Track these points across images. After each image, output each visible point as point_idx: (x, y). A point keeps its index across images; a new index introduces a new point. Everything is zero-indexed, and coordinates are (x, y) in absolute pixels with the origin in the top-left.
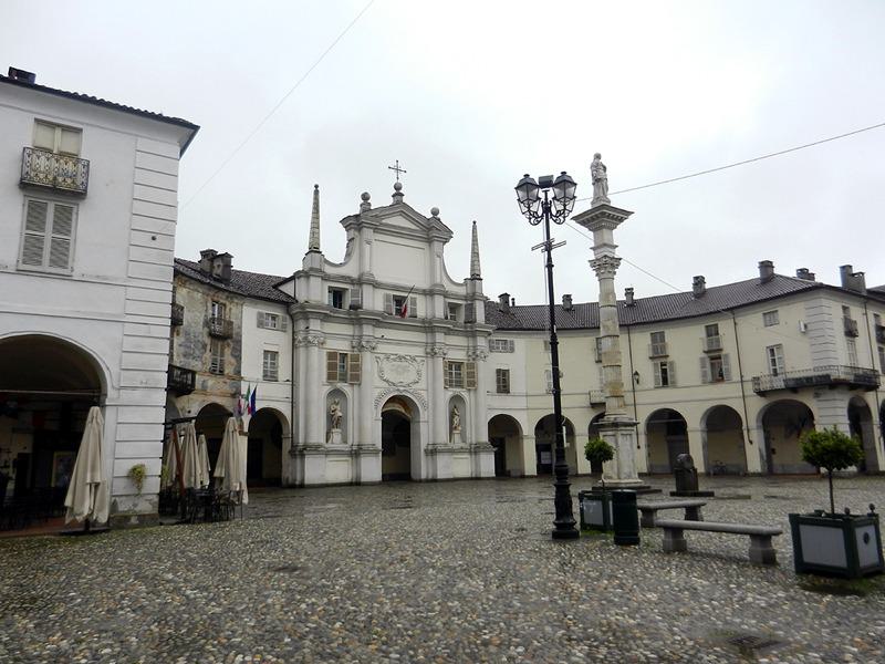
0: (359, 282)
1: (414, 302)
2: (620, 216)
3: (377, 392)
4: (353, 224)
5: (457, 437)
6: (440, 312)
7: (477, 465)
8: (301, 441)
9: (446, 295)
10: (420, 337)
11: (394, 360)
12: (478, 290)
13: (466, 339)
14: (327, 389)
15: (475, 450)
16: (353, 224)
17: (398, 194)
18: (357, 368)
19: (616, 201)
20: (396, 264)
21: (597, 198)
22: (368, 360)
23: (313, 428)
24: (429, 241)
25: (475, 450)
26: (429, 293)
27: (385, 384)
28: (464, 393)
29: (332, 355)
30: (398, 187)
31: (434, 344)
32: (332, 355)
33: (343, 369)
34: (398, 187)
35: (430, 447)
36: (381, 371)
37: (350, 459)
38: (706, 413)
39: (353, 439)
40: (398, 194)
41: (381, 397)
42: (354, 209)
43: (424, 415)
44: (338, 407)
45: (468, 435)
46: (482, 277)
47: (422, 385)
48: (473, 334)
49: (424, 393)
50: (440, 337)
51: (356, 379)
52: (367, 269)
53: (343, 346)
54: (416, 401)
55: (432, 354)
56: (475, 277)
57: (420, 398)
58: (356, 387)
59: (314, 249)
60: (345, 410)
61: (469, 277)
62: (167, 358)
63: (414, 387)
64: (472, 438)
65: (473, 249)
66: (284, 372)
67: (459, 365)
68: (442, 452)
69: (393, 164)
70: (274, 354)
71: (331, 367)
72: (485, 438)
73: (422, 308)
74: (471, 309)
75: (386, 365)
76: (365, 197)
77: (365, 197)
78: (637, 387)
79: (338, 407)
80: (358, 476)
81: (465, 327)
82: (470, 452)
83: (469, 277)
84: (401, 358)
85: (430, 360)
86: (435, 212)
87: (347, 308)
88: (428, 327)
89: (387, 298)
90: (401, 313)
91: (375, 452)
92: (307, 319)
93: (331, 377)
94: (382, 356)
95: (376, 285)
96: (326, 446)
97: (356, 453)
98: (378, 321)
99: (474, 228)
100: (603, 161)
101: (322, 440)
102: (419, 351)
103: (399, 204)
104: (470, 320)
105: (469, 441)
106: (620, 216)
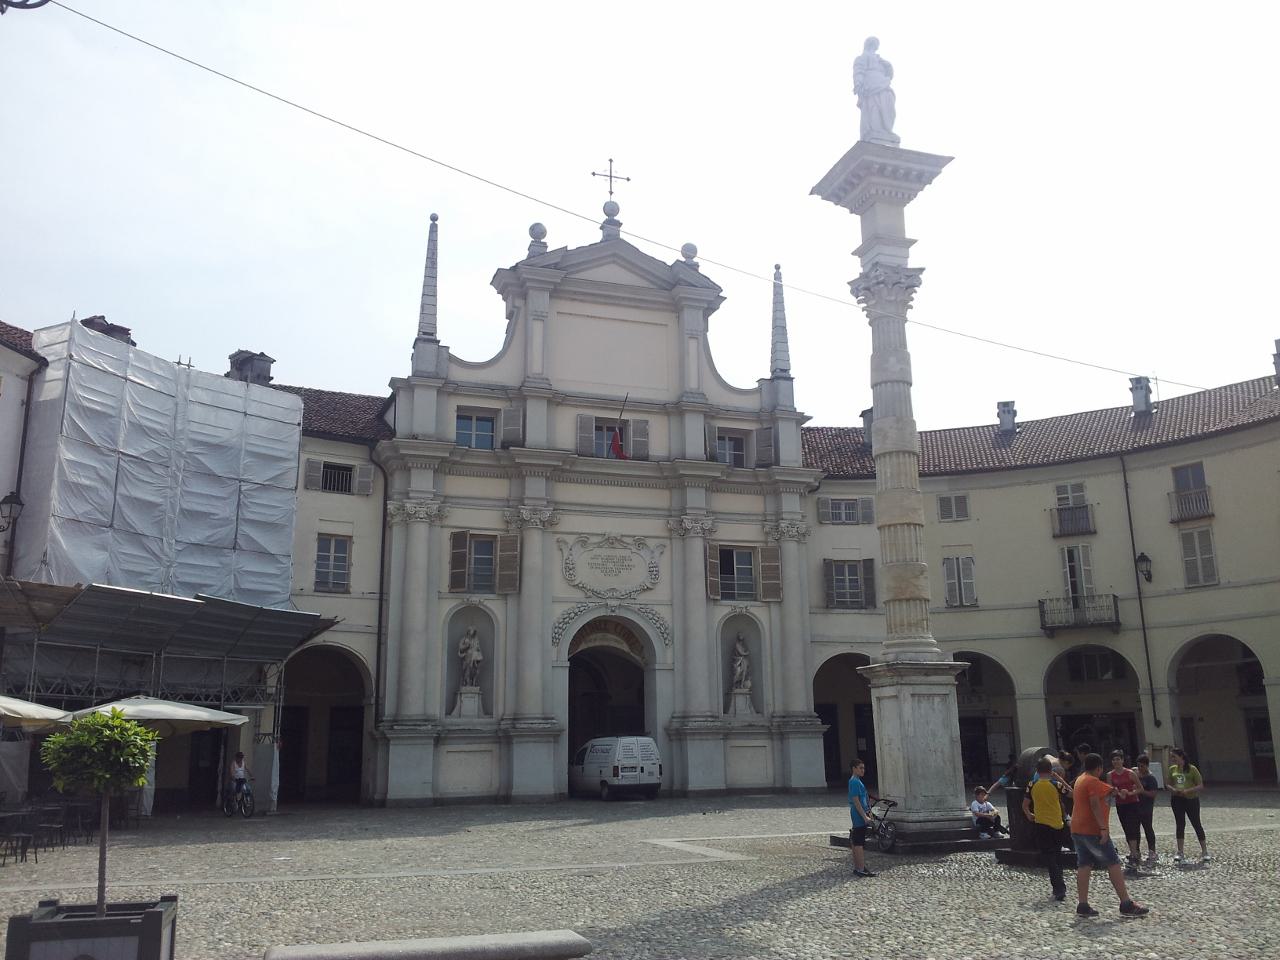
0: (518, 395)
1: (643, 430)
2: (922, 170)
3: (559, 611)
4: (511, 283)
5: (741, 702)
6: (695, 446)
7: (784, 761)
8: (389, 709)
9: (710, 413)
10: (659, 498)
11: (599, 545)
12: (782, 400)
13: (760, 499)
14: (449, 606)
15: (781, 729)
16: (511, 283)
17: (611, 224)
18: (516, 563)
19: (912, 133)
20: (603, 358)
21: (866, 128)
22: (536, 546)
23: (419, 682)
24: (676, 308)
25: (781, 729)
26: (675, 410)
27: (579, 595)
28: (758, 611)
29: (459, 539)
30: (611, 209)
31: (683, 510)
32: (459, 539)
33: (483, 565)
34: (611, 209)
35: (676, 724)
36: (569, 569)
37: (494, 747)
38: (1189, 643)
39: (502, 706)
40: (611, 224)
41: (567, 619)
42: (516, 252)
43: (664, 656)
44: (475, 643)
45: (768, 696)
46: (792, 373)
47: (662, 592)
48: (773, 490)
49: (664, 612)
50: (696, 498)
51: (512, 584)
52: (536, 368)
53: (485, 521)
54: (641, 623)
55: (680, 532)
56: (781, 375)
57: (655, 619)
58: (511, 601)
59: (427, 336)
60: (487, 649)
61: (768, 375)
62: (1038, 610)
63: (643, 598)
64: (773, 702)
65: (775, 320)
66: (362, 572)
67: (486, 543)
68: (699, 733)
69: (617, 171)
70: (344, 543)
71: (457, 561)
72: (802, 700)
73: (659, 440)
74: (770, 440)
75: (582, 559)
76: (537, 232)
77: (537, 232)
78: (1146, 587)
79: (475, 643)
80: (509, 785)
81: (756, 476)
82: (770, 735)
83: (768, 375)
84: (611, 541)
85: (677, 544)
86: (689, 251)
87: (753, 465)
88: (672, 475)
89: (582, 424)
90: (618, 451)
91: (553, 736)
92: (408, 470)
93: (457, 583)
94: (571, 539)
95: (557, 399)
96: (449, 720)
97: (505, 737)
98: (561, 467)
99: (433, 229)
100: (883, 52)
101: (436, 709)
102: (653, 527)
103: (612, 245)
104: (769, 461)
105: (768, 710)
106: (922, 170)
